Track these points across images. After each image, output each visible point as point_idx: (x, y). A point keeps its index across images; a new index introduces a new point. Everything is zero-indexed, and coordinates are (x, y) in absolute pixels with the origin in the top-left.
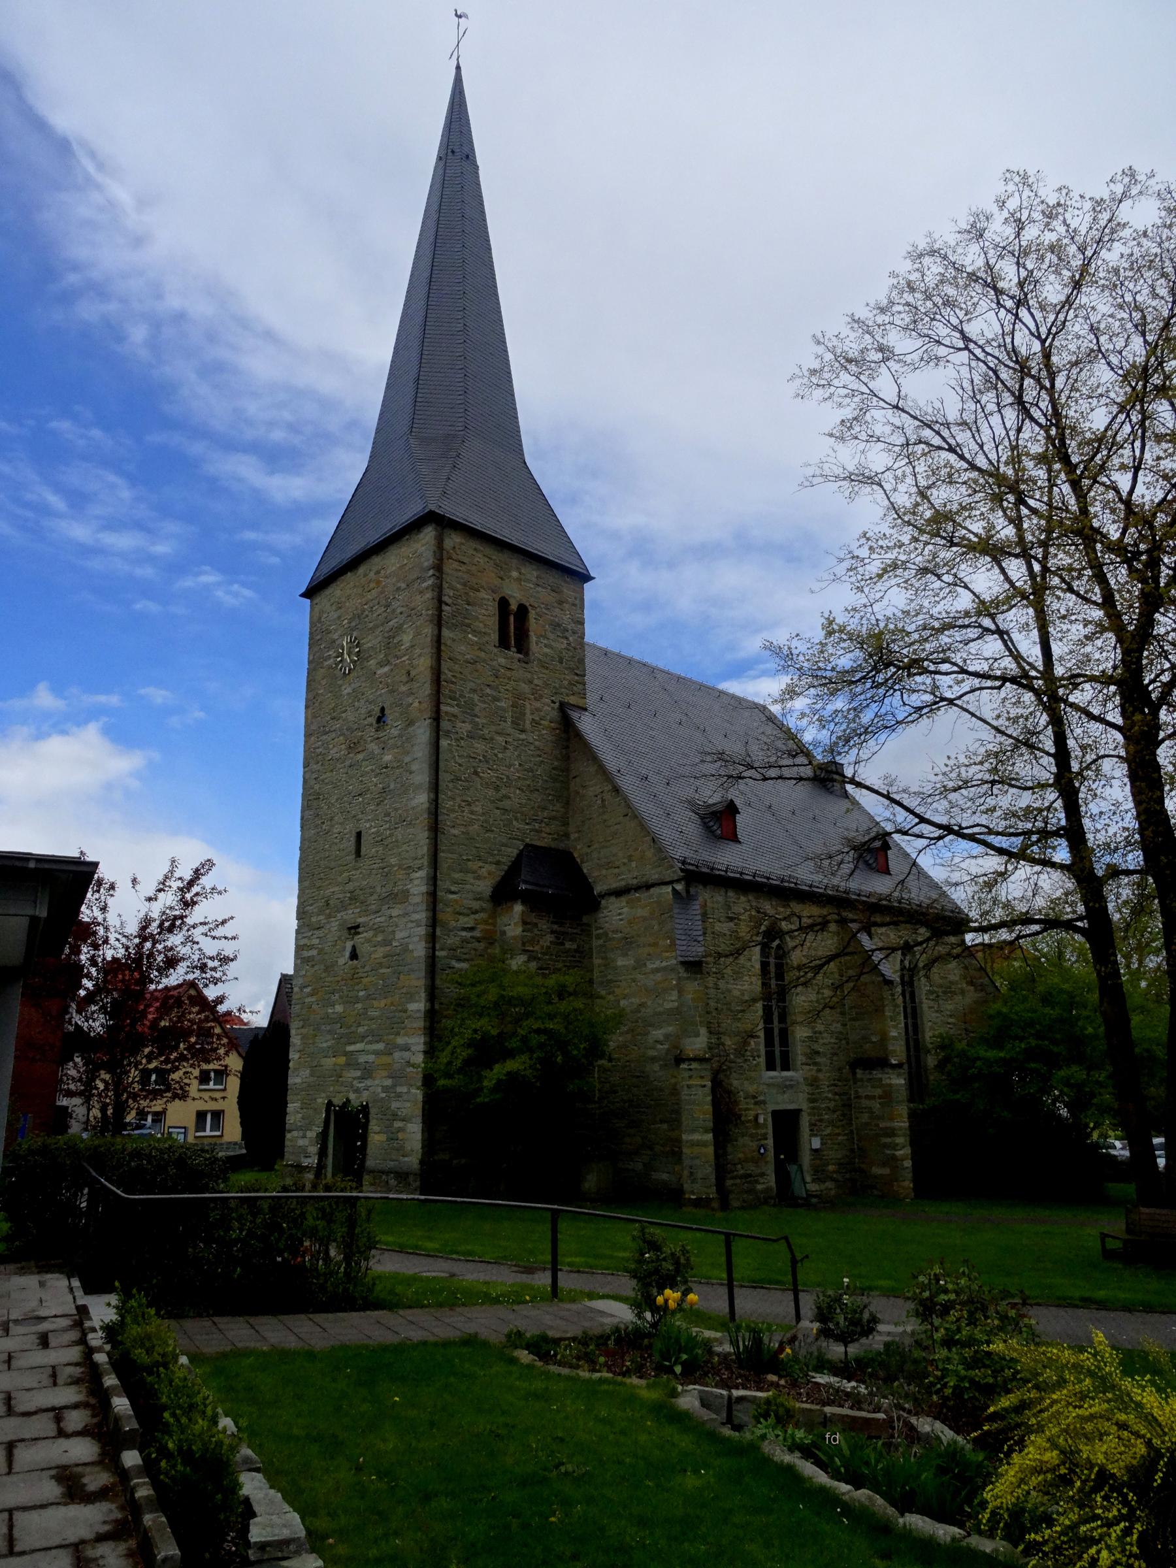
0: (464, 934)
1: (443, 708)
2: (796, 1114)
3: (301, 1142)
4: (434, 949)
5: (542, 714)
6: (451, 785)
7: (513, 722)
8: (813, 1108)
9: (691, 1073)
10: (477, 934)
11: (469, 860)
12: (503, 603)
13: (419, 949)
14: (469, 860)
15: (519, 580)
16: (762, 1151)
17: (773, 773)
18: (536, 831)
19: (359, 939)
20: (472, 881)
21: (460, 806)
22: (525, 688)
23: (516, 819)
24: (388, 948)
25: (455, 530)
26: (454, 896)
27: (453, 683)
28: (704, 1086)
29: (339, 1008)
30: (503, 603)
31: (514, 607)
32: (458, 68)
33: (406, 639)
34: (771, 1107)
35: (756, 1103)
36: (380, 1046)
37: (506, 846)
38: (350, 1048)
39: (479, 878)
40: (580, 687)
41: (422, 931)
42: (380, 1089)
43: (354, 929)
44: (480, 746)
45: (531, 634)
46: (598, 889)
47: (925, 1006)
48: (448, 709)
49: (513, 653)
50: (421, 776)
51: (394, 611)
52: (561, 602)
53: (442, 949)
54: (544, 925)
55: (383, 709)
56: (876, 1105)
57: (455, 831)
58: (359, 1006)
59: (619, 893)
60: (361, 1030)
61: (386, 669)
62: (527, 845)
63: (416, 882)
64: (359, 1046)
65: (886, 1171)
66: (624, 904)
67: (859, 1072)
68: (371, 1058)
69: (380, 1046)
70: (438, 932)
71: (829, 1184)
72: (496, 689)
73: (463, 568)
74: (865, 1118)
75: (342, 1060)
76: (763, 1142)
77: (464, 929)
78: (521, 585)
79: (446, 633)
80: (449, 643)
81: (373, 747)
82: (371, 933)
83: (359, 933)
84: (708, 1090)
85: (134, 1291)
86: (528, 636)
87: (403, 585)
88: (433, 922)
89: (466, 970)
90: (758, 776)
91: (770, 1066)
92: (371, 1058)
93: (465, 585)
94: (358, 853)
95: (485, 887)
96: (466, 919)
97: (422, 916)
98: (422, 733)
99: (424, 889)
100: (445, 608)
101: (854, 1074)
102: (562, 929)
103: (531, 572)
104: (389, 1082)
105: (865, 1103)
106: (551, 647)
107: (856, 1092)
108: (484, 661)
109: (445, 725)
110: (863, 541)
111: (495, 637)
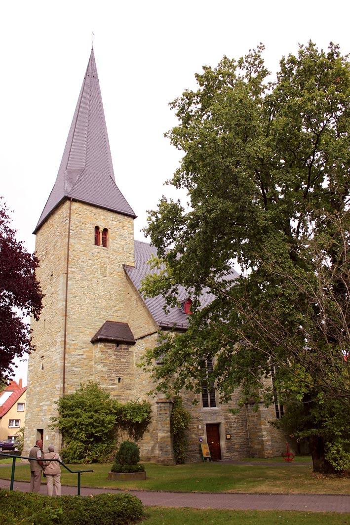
0: (79, 357)
1: (69, 269)
2: (218, 425)
5: (114, 269)
6: (73, 299)
7: (101, 273)
8: (226, 422)
9: (161, 408)
10: (84, 356)
11: (81, 328)
12: (97, 228)
13: (60, 363)
14: (81, 328)
16: (201, 440)
18: (111, 315)
19: (44, 361)
20: (82, 336)
22: (107, 260)
24: (51, 364)
25: (76, 202)
26: (74, 342)
28: (166, 413)
31: (101, 229)
33: (59, 244)
34: (205, 422)
35: (198, 421)
36: (49, 403)
37: (97, 321)
39: (85, 335)
44: (86, 283)
46: (136, 337)
48: (73, 269)
49: (101, 247)
50: (62, 296)
52: (123, 227)
53: (69, 363)
54: (111, 352)
56: (255, 419)
57: (75, 317)
58: (43, 387)
59: (141, 338)
60: (44, 397)
62: (107, 321)
65: (260, 447)
66: (143, 342)
69: (49, 403)
70: (66, 356)
71: (236, 453)
72: (93, 261)
73: (80, 216)
74: (251, 425)
77: (79, 355)
78: (105, 220)
79: (71, 240)
80: (73, 244)
83: (44, 359)
84: (168, 415)
85: (336, 469)
89: (79, 371)
91: (205, 404)
93: (80, 222)
96: (80, 351)
98: (62, 279)
100: (71, 231)
101: (247, 407)
102: (120, 354)
103: (111, 216)
105: (251, 419)
106: (118, 244)
107: (248, 415)
108: (88, 250)
109: (69, 275)
111: (93, 241)
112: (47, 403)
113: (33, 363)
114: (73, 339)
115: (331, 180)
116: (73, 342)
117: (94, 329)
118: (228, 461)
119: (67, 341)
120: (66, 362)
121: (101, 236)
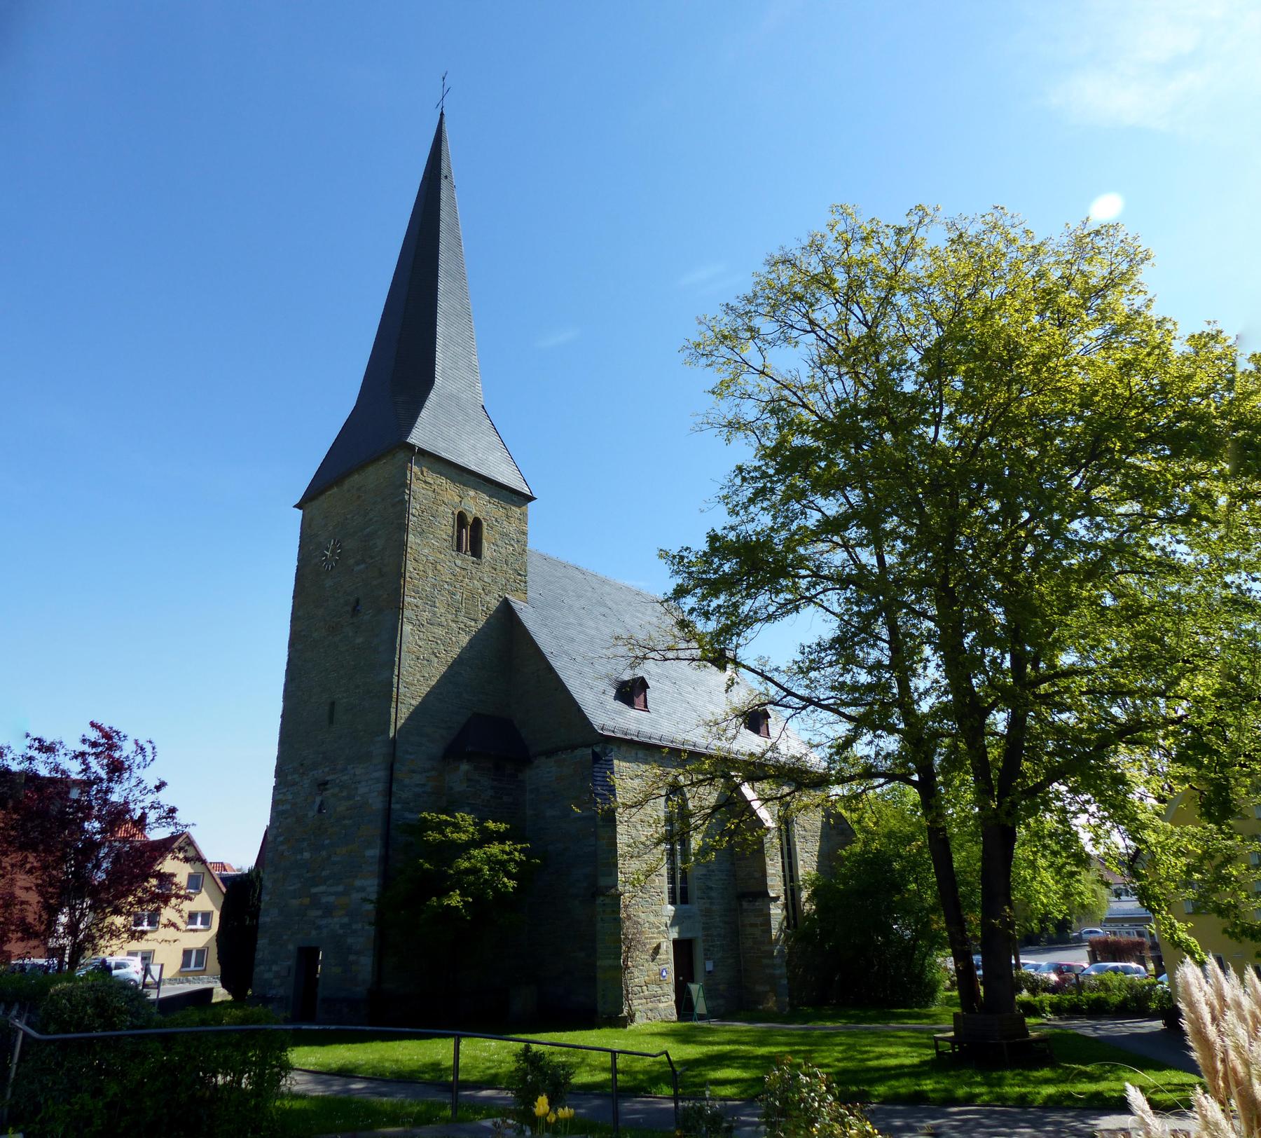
3: (267, 976)
12: (461, 518)
13: (377, 803)
15: (474, 498)
29: (307, 855)
30: (461, 518)
31: (470, 520)
32: (442, 114)
36: (340, 888)
38: (314, 890)
41: (381, 787)
43: (323, 785)
55: (357, 601)
59: (549, 753)
61: (362, 566)
64: (322, 888)
67: (745, 905)
69: (340, 888)
75: (307, 901)
78: (477, 504)
86: (481, 543)
92: (331, 899)
94: (331, 721)
97: (381, 774)
104: (346, 920)
112: (333, 889)
120: (393, 800)
121: (470, 535)
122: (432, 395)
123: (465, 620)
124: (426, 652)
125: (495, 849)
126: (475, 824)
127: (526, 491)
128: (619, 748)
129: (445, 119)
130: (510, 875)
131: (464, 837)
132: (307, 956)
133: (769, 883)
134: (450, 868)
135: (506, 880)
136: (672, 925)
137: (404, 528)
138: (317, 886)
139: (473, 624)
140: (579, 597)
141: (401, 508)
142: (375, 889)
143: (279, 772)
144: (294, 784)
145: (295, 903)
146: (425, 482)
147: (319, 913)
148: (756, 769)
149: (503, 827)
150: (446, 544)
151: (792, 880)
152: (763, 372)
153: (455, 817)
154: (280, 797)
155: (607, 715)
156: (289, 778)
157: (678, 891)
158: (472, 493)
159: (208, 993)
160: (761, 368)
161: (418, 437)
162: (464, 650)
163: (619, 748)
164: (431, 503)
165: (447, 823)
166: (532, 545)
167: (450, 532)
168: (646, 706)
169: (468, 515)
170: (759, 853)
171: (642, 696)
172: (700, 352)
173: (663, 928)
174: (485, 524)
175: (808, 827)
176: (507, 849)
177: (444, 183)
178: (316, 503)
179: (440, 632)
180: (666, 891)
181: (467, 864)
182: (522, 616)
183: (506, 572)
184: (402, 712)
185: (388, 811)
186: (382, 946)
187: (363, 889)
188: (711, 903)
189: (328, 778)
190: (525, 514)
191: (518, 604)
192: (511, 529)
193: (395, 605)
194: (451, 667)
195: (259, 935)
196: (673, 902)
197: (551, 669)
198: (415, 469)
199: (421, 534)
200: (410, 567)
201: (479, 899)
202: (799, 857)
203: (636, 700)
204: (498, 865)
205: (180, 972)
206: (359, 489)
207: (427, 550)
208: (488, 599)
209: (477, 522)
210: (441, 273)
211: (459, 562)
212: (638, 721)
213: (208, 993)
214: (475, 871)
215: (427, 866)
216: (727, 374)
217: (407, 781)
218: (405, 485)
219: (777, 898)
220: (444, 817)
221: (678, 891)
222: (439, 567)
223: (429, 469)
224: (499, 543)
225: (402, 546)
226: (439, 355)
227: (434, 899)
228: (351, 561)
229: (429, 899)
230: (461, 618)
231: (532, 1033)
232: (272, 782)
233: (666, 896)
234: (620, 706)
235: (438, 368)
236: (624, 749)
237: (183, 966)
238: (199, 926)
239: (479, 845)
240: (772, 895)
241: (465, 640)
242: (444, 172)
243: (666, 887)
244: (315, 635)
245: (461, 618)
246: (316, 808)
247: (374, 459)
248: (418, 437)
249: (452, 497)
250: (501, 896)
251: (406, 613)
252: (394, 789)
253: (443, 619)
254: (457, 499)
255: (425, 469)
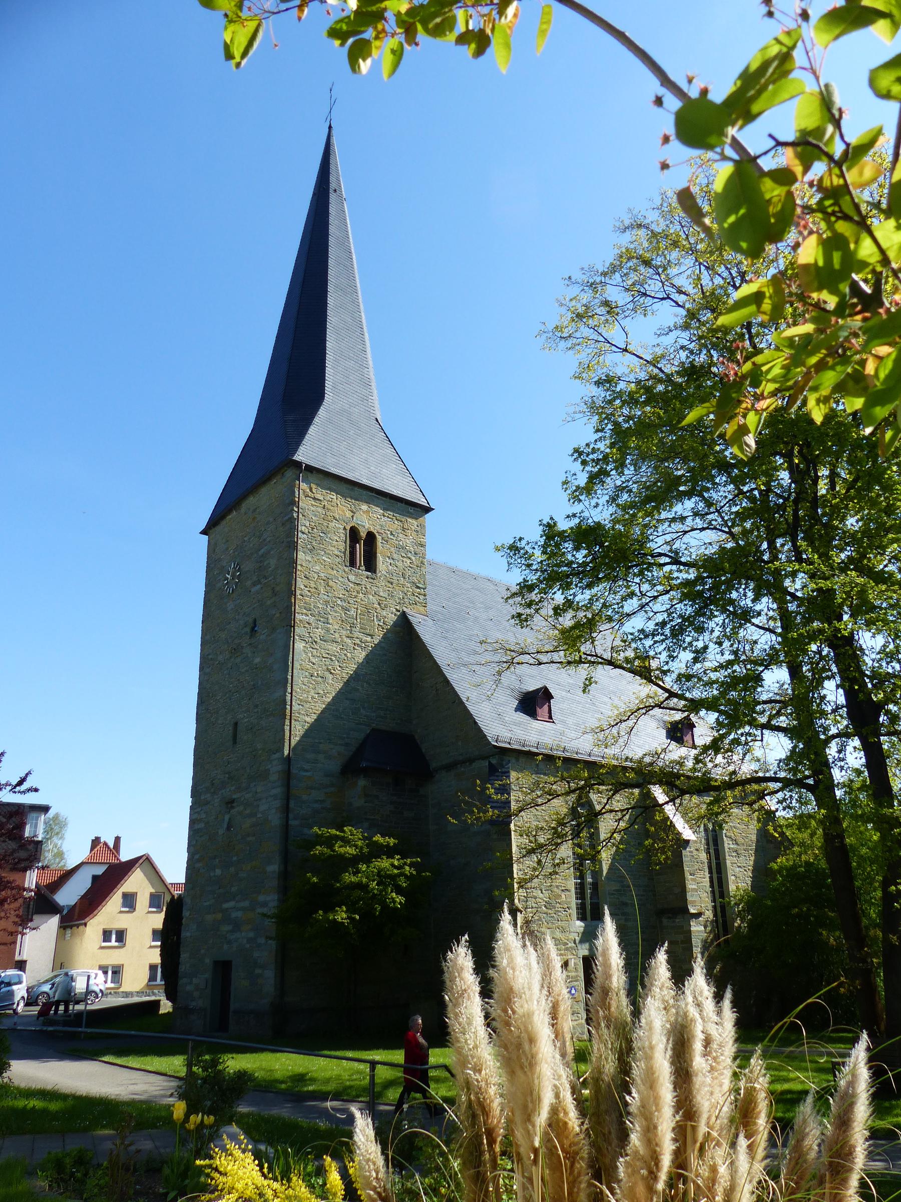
3: (188, 988)
4: (287, 818)
12: (354, 534)
13: (275, 819)
15: (367, 512)
17: (544, 658)
21: (313, 698)
23: (364, 708)
24: (254, 820)
25: (312, 472)
27: (307, 596)
29: (218, 872)
30: (354, 534)
31: (363, 535)
32: (330, 127)
36: (246, 904)
38: (226, 906)
40: (422, 597)
41: (277, 803)
42: (245, 941)
43: (230, 803)
45: (378, 555)
46: (434, 765)
47: (728, 862)
51: (265, 540)
55: (255, 621)
59: (449, 767)
61: (259, 587)
63: (275, 763)
64: (231, 904)
67: (665, 921)
68: (239, 914)
69: (246, 904)
75: (219, 916)
76: (575, 983)
77: (316, 801)
78: (369, 518)
81: (247, 651)
82: (241, 808)
86: (376, 557)
87: (271, 519)
88: (288, 796)
90: (532, 661)
92: (239, 914)
94: (235, 741)
95: (334, 766)
97: (278, 791)
99: (280, 768)
104: (251, 935)
110: (576, 455)
112: (242, 904)
113: (203, 816)
114: (306, 767)
115: (870, 918)
116: (305, 774)
117: (347, 745)
118: (55, 1116)
119: (294, 771)
120: (291, 816)
121: (363, 550)
122: (322, 412)
123: (361, 635)
124: (319, 672)
125: (384, 863)
126: (365, 838)
127: (422, 501)
128: (517, 760)
129: (334, 132)
130: (399, 890)
131: (351, 851)
132: (223, 968)
133: (689, 898)
134: (339, 882)
135: (394, 895)
136: (581, 942)
137: (293, 546)
138: (227, 901)
139: (369, 639)
140: (488, 608)
141: (291, 525)
142: (275, 904)
143: (195, 793)
144: (207, 803)
145: (209, 918)
146: (314, 499)
147: (230, 928)
148: (676, 783)
149: (392, 841)
150: (338, 560)
151: (722, 895)
152: (626, 350)
153: (344, 832)
154: (196, 816)
155: (502, 723)
156: (202, 798)
157: (588, 907)
158: (364, 507)
159: (157, 1004)
160: (623, 346)
161: (303, 455)
162: (361, 666)
163: (517, 760)
164: (322, 518)
165: (337, 838)
166: (431, 554)
167: (342, 548)
168: (550, 717)
169: (361, 529)
170: (677, 866)
171: (546, 707)
172: (559, 334)
173: (571, 945)
174: (379, 538)
175: (741, 840)
176: (396, 863)
177: (333, 197)
178: (218, 528)
179: (334, 648)
180: (574, 906)
181: (353, 879)
182: (419, 629)
183: (403, 586)
184: (296, 730)
185: (286, 826)
186: (283, 960)
187: (264, 904)
188: (626, 920)
189: (235, 796)
190: (422, 526)
191: (416, 619)
192: (408, 541)
193: (288, 624)
194: (347, 684)
195: (182, 949)
196: (582, 917)
197: (447, 682)
198: (304, 486)
199: (311, 551)
200: (300, 583)
201: (367, 914)
202: (730, 872)
203: (539, 711)
204: (383, 878)
205: (147, 985)
206: (255, 510)
207: (319, 565)
208: (384, 613)
209: (371, 537)
210: (331, 288)
211: (352, 578)
212: (541, 733)
213: (157, 1004)
214: (360, 886)
215: (315, 879)
216: (584, 355)
217: (305, 797)
218: (294, 503)
219: (699, 915)
220: (334, 832)
221: (588, 907)
222: (331, 583)
223: (317, 485)
224: (395, 556)
225: (292, 563)
226: (329, 371)
227: (321, 912)
228: (249, 583)
229: (317, 912)
230: (356, 634)
231: (335, 1050)
232: (188, 801)
233: (574, 912)
234: (522, 717)
235: (328, 384)
236: (522, 760)
237: (150, 980)
238: (113, 943)
239: (367, 859)
240: (692, 911)
241: (361, 655)
242: (333, 185)
243: (574, 903)
244: (220, 658)
245: (356, 634)
246: (225, 826)
247: (265, 481)
248: (303, 455)
249: (346, 512)
250: (389, 912)
251: (298, 630)
252: (292, 804)
253: (337, 635)
254: (349, 514)
255: (313, 486)
